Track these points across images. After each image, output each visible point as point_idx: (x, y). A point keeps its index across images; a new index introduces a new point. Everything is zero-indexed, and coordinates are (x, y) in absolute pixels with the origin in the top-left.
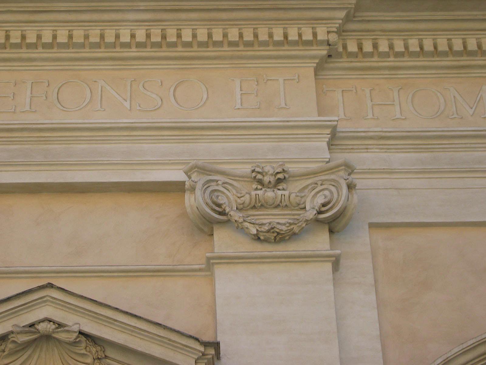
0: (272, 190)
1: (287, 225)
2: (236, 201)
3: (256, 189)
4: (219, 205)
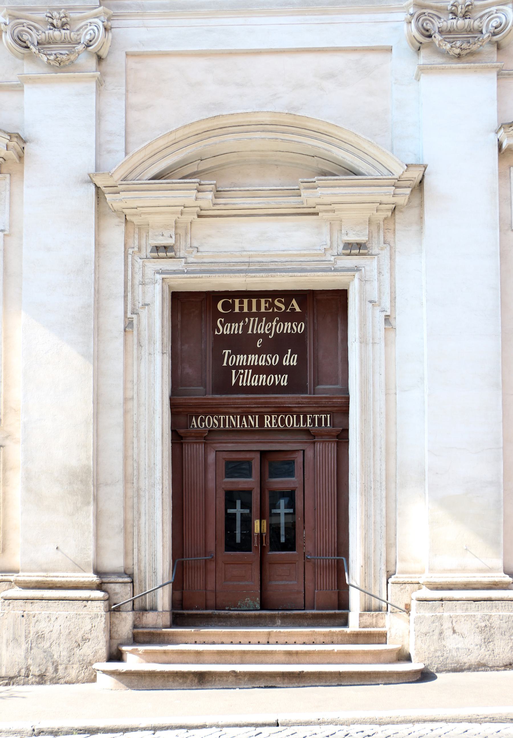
0: (59, 30)
1: (66, 55)
2: (37, 38)
3: (50, 29)
4: (427, 31)
